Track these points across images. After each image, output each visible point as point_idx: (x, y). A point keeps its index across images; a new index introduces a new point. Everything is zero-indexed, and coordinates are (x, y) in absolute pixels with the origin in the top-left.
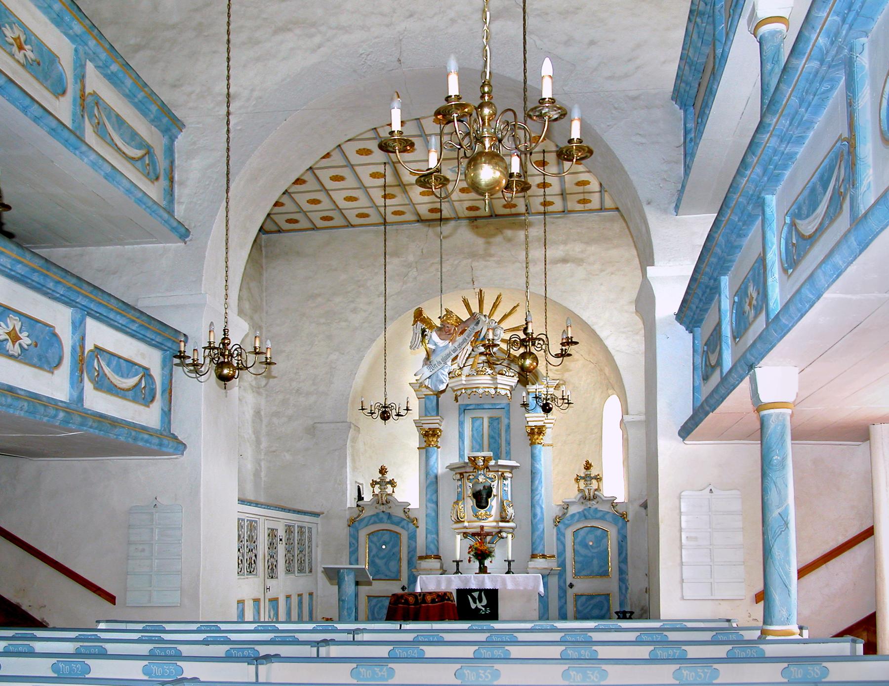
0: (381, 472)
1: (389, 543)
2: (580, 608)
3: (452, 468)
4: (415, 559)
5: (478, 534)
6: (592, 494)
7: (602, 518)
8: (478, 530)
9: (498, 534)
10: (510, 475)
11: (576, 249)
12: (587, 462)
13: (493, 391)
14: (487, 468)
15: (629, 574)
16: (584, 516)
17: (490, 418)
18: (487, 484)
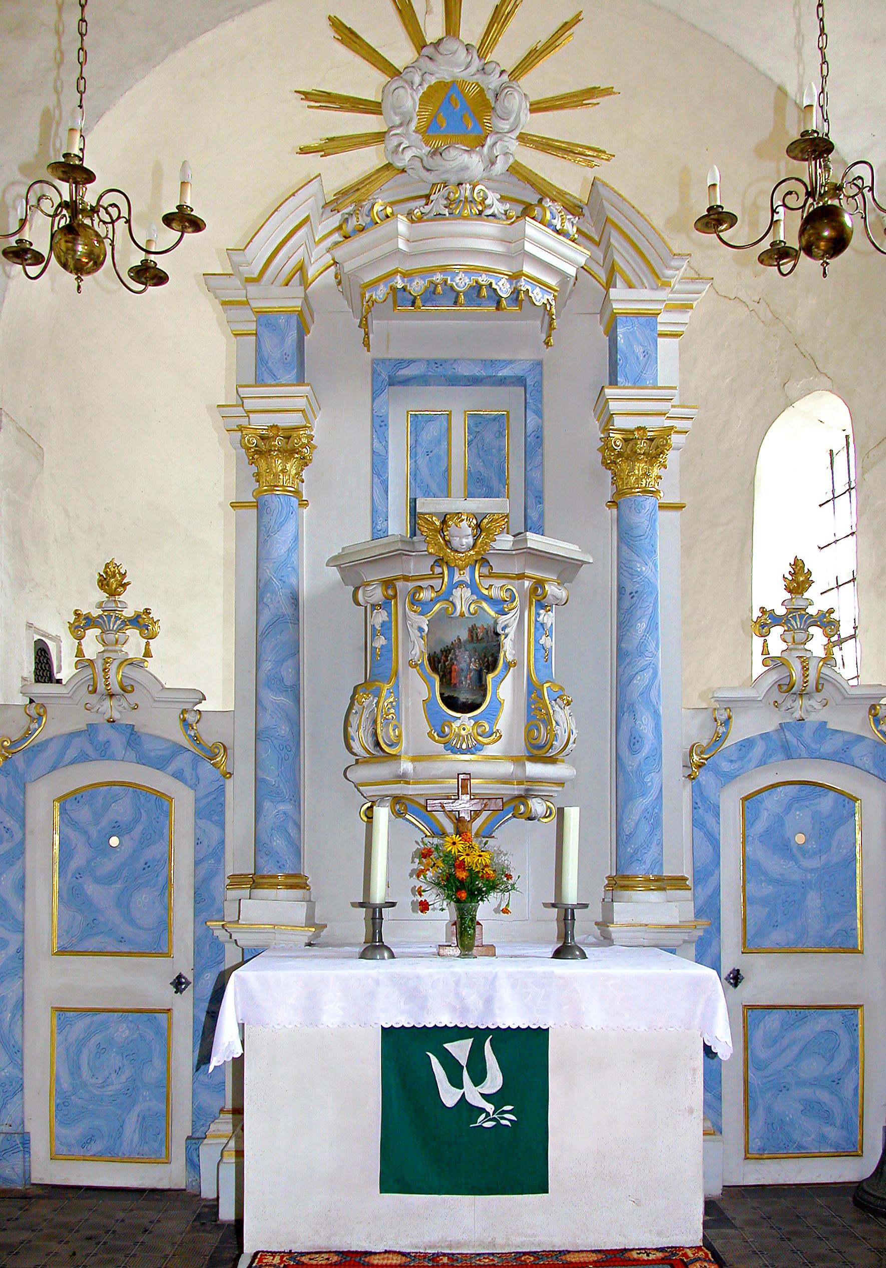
0: (103, 583)
1: (129, 830)
2: (762, 1054)
3: (351, 568)
7: (842, 757)
12: (798, 566)
13: (504, 289)
14: (484, 561)
16: (783, 744)
18: (487, 623)
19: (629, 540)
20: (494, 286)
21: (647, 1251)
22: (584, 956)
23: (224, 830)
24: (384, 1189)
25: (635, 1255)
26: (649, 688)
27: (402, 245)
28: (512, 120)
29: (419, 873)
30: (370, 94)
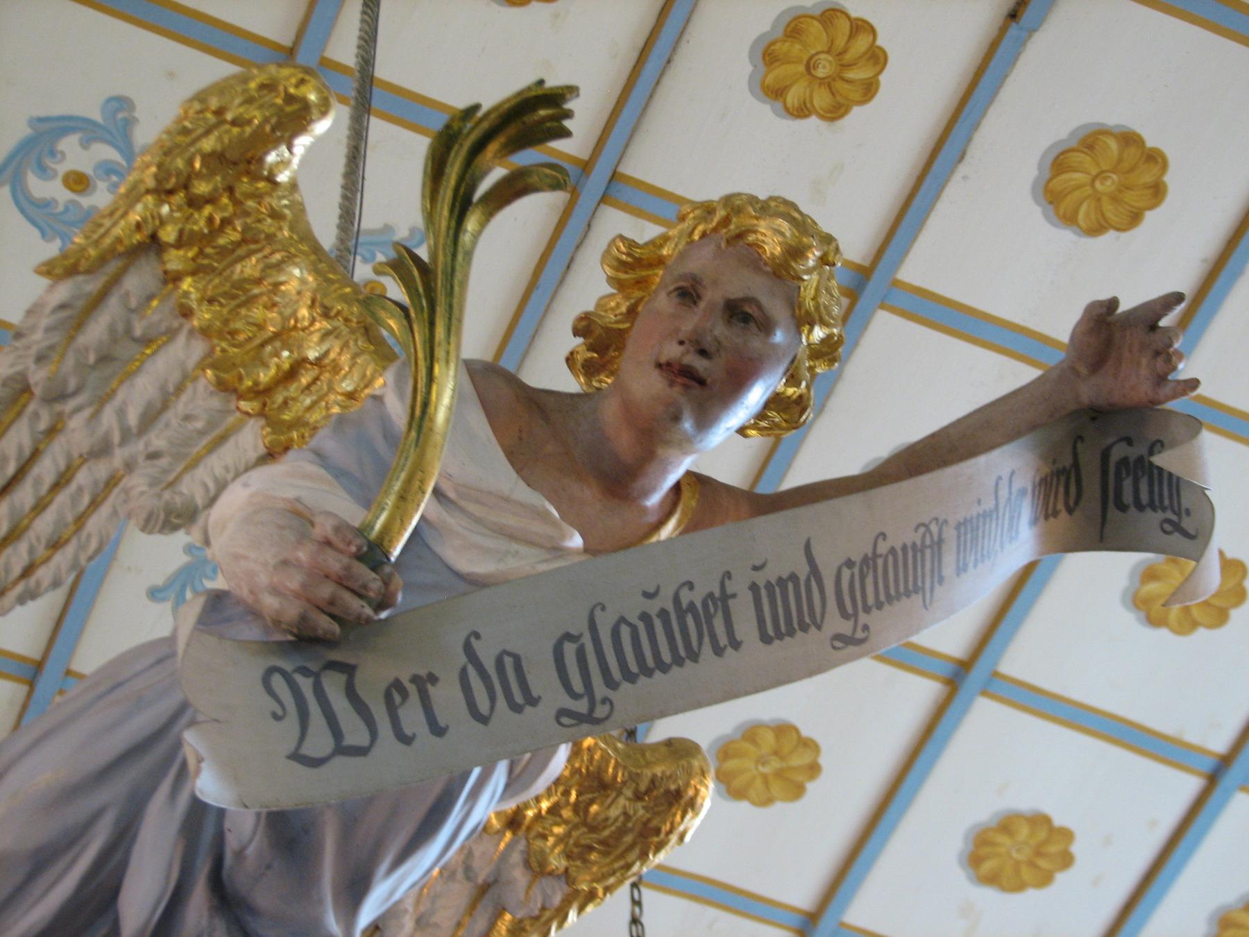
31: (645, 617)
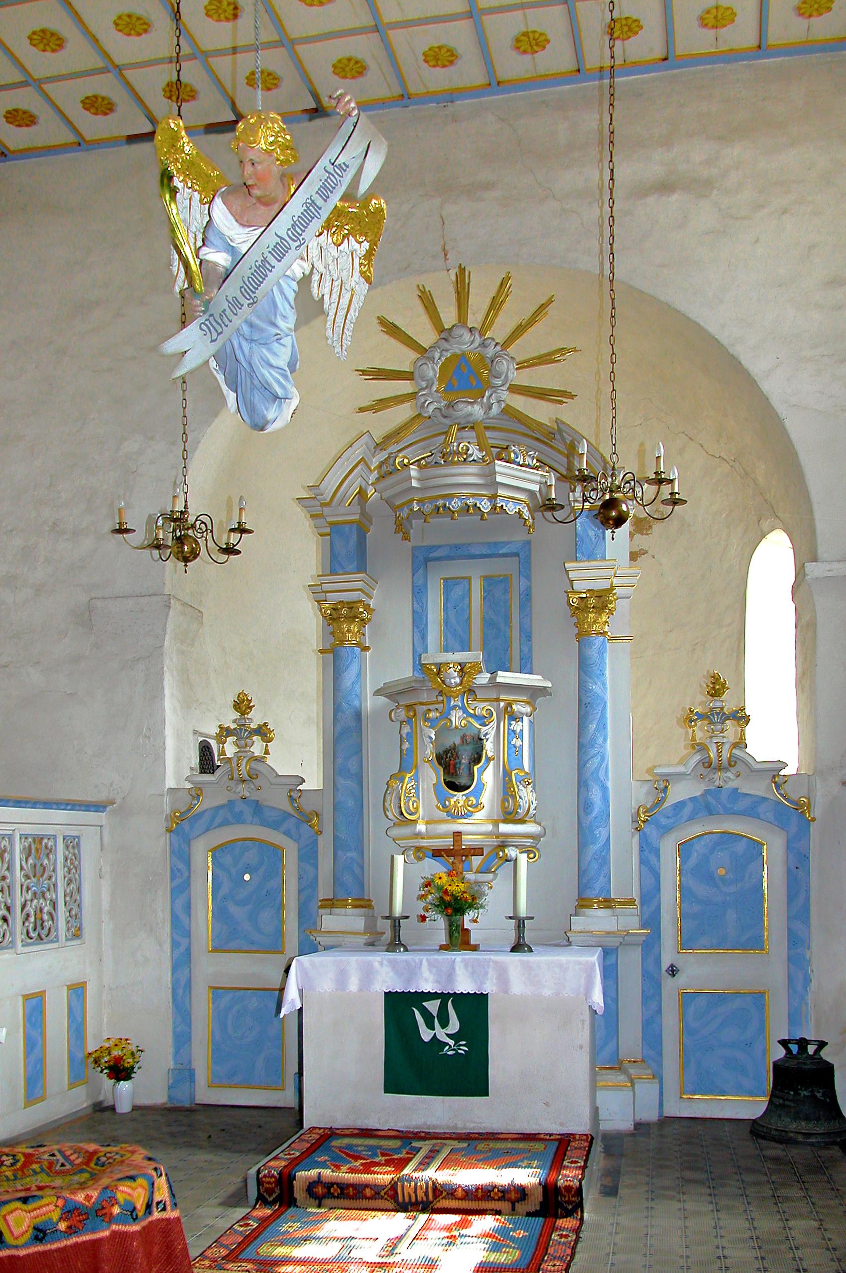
0: (237, 706)
3: (391, 692)
4: (314, 905)
5: (449, 852)
6: (725, 755)
8: (448, 842)
9: (497, 852)
10: (528, 709)
11: (695, 155)
12: (715, 679)
14: (471, 691)
15: (814, 945)
16: (705, 806)
17: (486, 578)
19: (586, 668)
20: (478, 505)
21: (551, 1135)
22: (530, 950)
23: (317, 869)
24: (387, 1090)
25: (542, 1136)
26: (598, 769)
27: (415, 484)
28: (503, 378)
29: (421, 897)
30: (406, 367)
31: (252, 274)
